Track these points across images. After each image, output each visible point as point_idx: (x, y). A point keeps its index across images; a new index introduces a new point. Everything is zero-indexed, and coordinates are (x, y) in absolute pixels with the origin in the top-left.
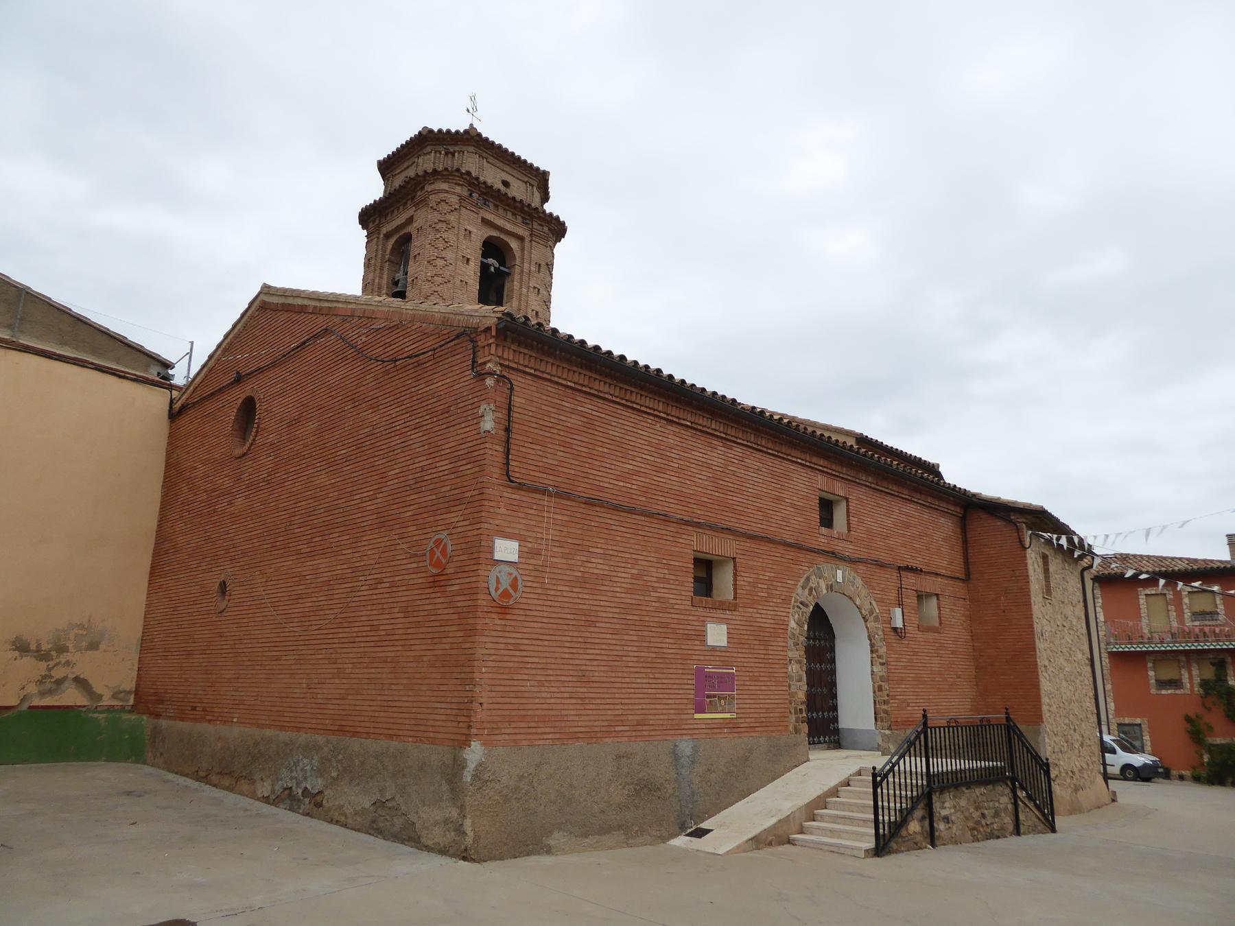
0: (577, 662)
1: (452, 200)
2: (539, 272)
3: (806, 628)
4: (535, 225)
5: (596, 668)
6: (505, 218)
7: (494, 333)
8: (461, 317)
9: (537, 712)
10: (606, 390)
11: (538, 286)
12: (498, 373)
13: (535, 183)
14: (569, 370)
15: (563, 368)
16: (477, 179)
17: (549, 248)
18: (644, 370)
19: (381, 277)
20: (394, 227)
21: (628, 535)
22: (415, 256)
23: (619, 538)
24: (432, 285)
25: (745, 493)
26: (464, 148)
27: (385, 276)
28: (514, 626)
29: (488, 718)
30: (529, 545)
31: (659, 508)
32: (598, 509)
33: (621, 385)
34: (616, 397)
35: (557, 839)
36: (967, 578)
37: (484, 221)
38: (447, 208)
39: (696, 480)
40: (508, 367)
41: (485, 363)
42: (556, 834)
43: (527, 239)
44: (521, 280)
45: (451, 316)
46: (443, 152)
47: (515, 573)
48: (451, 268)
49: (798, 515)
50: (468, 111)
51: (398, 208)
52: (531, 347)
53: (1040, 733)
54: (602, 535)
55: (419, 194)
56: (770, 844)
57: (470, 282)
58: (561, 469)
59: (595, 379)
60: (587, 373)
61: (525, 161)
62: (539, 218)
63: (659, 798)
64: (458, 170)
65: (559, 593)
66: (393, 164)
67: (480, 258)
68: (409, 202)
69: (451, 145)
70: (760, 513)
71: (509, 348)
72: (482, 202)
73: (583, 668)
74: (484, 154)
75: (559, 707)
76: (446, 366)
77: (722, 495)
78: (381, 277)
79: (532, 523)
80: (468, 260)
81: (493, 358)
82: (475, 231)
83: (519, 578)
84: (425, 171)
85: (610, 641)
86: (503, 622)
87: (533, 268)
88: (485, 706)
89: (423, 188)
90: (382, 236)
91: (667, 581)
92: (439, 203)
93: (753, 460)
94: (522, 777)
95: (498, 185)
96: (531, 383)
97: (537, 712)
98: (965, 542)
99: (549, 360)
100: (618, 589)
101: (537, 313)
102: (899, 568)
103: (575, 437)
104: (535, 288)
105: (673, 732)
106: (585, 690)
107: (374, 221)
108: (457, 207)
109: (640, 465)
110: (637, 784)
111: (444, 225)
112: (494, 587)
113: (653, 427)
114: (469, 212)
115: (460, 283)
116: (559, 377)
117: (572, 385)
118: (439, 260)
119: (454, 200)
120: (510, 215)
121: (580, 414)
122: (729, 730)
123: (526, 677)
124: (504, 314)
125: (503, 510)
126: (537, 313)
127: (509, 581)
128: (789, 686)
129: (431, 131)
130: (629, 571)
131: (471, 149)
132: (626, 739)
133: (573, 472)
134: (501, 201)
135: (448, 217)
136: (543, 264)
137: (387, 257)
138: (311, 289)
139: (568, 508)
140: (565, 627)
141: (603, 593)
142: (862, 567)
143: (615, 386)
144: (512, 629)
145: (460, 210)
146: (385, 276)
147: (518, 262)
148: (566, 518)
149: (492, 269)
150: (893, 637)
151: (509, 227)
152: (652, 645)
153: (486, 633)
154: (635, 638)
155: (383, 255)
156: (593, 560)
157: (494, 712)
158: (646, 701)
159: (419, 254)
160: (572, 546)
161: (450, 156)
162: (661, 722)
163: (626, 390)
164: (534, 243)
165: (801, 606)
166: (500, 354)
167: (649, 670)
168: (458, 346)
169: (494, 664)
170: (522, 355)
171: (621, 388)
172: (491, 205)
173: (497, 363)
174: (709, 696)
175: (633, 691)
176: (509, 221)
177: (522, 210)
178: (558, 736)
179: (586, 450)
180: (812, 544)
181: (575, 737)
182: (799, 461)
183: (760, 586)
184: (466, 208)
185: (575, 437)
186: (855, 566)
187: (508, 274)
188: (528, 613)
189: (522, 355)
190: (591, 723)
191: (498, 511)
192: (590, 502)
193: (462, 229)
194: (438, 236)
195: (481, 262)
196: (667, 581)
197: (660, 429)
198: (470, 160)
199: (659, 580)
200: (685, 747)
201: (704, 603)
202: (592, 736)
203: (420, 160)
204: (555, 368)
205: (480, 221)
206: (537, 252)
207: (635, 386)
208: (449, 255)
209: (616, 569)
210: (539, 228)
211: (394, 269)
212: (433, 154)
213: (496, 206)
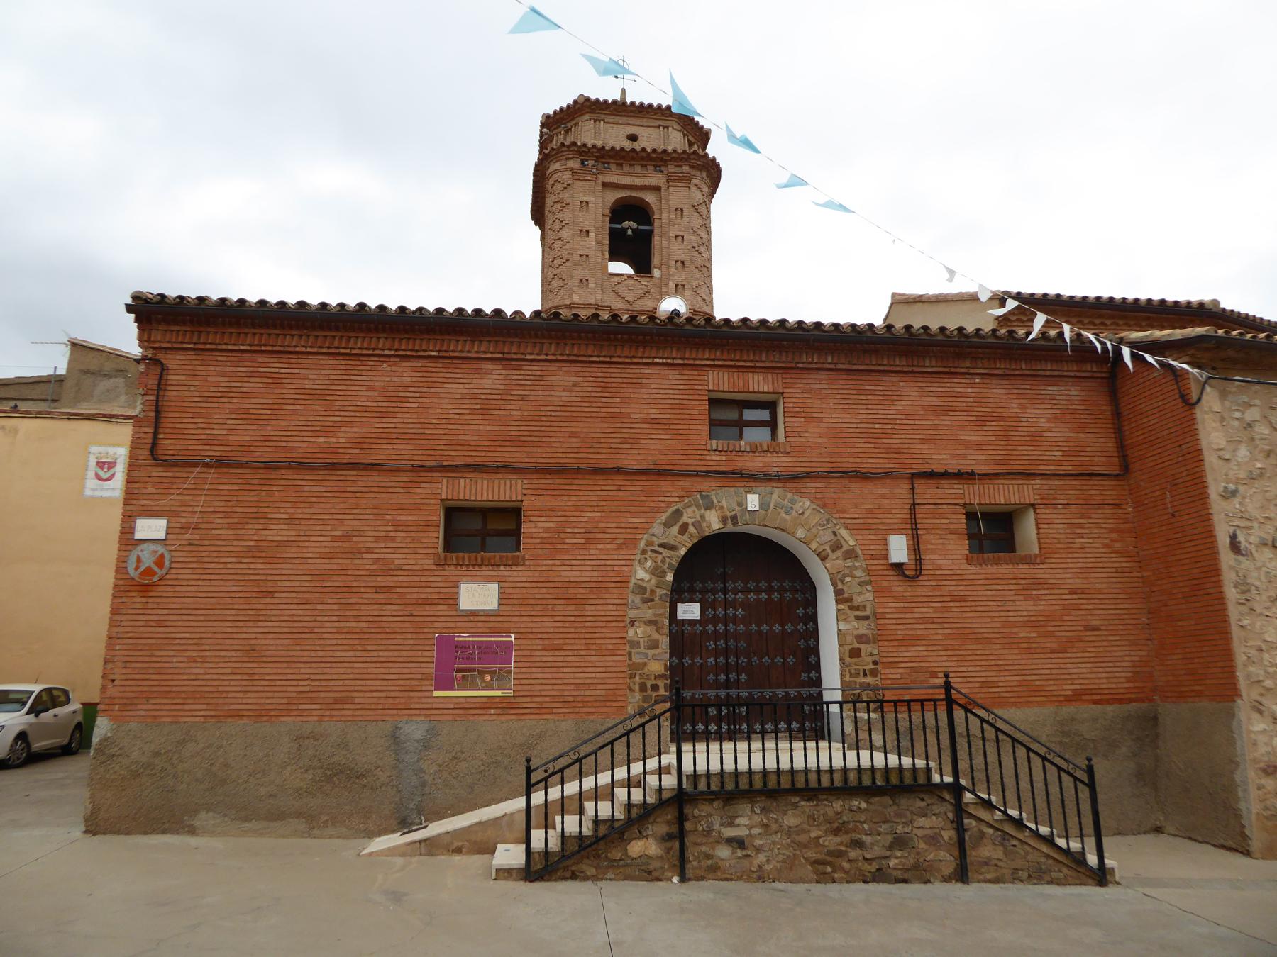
0: (244, 636)
3: (670, 577)
5: (272, 642)
6: (630, 174)
9: (184, 689)
12: (150, 356)
21: (329, 495)
23: (314, 499)
25: (544, 419)
28: (158, 603)
29: (120, 695)
30: (183, 520)
31: (381, 458)
32: (283, 472)
35: (203, 819)
36: (1124, 470)
37: (604, 185)
39: (451, 416)
42: (203, 815)
47: (161, 549)
48: (568, 246)
49: (660, 431)
52: (184, 323)
53: (1234, 715)
54: (288, 499)
56: (458, 851)
57: (591, 253)
58: (231, 437)
61: (650, 106)
62: (673, 159)
63: (365, 786)
65: (221, 566)
70: (574, 440)
73: (253, 642)
75: (216, 683)
77: (502, 428)
79: (187, 498)
80: (588, 232)
83: (167, 555)
85: (294, 612)
86: (144, 600)
87: (672, 216)
88: (116, 683)
91: (393, 539)
93: (560, 377)
94: (157, 754)
95: (628, 145)
96: (194, 357)
97: (184, 689)
98: (1117, 414)
99: (209, 329)
100: (310, 555)
101: (683, 262)
102: (914, 476)
103: (253, 401)
104: (677, 237)
105: (395, 712)
106: (255, 665)
109: (353, 414)
110: (327, 769)
112: (134, 566)
113: (380, 368)
114: (584, 183)
117: (248, 348)
119: (566, 176)
121: (262, 375)
122: (499, 711)
123: (171, 653)
125: (151, 490)
127: (153, 559)
128: (630, 655)
130: (328, 533)
131: (587, 117)
132: (316, 719)
133: (248, 438)
134: (623, 158)
136: (686, 208)
138: (937, 292)
139: (241, 476)
140: (229, 600)
141: (288, 561)
142: (812, 486)
144: (155, 606)
148: (236, 487)
149: (630, 232)
150: (895, 578)
151: (638, 181)
152: (363, 613)
153: (124, 611)
154: (335, 607)
156: (273, 527)
157: (127, 689)
158: (351, 676)
160: (243, 515)
162: (375, 700)
165: (661, 550)
167: (356, 642)
169: (131, 641)
172: (613, 167)
174: (459, 671)
175: (329, 665)
176: (637, 175)
177: (651, 159)
178: (212, 713)
179: (269, 412)
180: (694, 464)
181: (237, 714)
182: (657, 360)
183: (569, 530)
185: (253, 401)
186: (795, 485)
188: (178, 588)
190: (263, 701)
191: (145, 491)
192: (272, 466)
196: (393, 539)
197: (389, 369)
199: (377, 539)
200: (415, 730)
201: (479, 559)
202: (261, 714)
205: (600, 187)
206: (677, 197)
208: (565, 233)
209: (307, 533)
210: (678, 170)
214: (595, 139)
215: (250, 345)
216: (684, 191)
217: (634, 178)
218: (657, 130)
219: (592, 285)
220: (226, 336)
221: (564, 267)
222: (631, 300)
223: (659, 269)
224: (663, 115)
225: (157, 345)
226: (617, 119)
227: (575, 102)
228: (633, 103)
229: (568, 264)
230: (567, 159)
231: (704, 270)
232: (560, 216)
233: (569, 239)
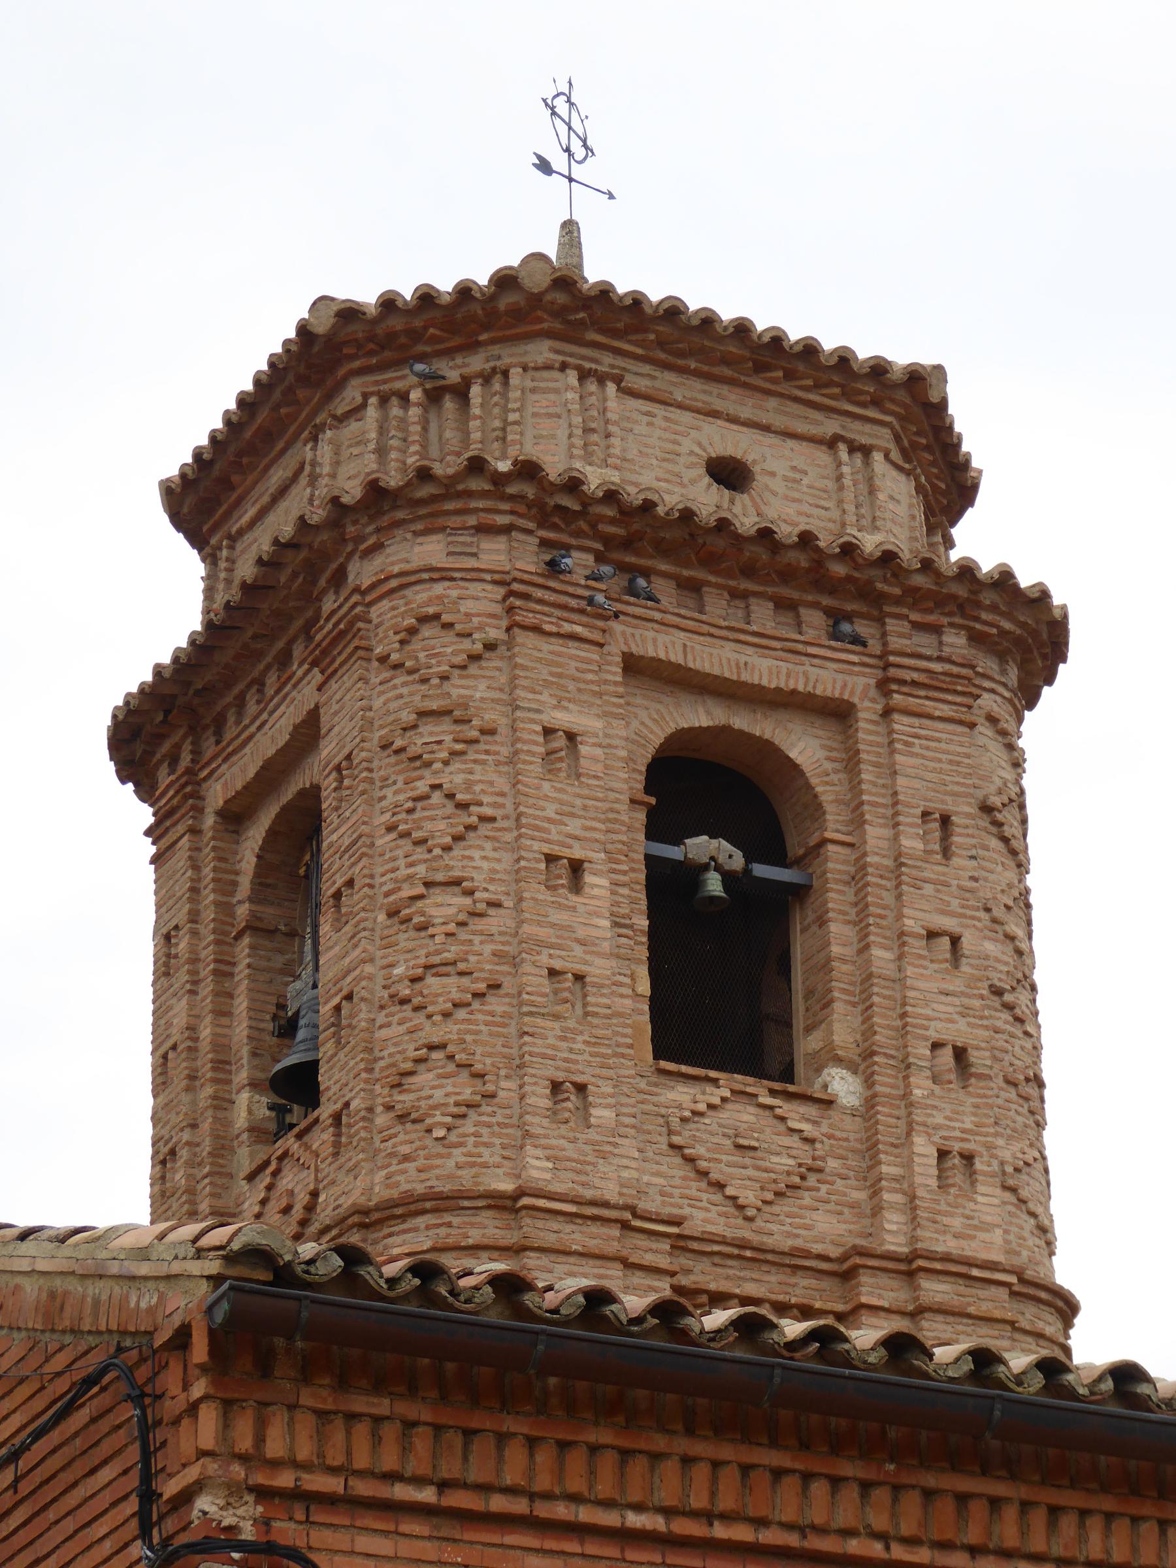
1: (467, 606)
2: (946, 852)
4: (900, 635)
6: (736, 635)
7: (200, 1351)
8: (94, 1289)
10: (844, 1516)
11: (948, 923)
12: (248, 1533)
13: (882, 437)
14: (625, 1454)
15: (594, 1449)
16: (573, 485)
17: (984, 729)
18: (1037, 1381)
19: (222, 1013)
20: (251, 773)
22: (337, 895)
24: (419, 1018)
26: (508, 355)
27: (241, 1004)
33: (930, 1480)
34: (911, 1542)
38: (451, 648)
40: (298, 1495)
41: (186, 1497)
43: (867, 711)
44: (861, 904)
45: (73, 1285)
46: (415, 395)
48: (496, 922)
50: (544, 166)
51: (260, 683)
55: (328, 605)
57: (599, 968)
59: (778, 1474)
60: (726, 1452)
61: (810, 349)
62: (914, 598)
64: (477, 465)
66: (226, 484)
67: (640, 845)
68: (298, 651)
69: (449, 353)
71: (292, 1407)
72: (618, 583)
74: (606, 363)
76: (69, 1525)
78: (222, 1013)
80: (577, 868)
81: (212, 1467)
82: (597, 724)
84: (335, 501)
87: (911, 843)
89: (339, 577)
90: (209, 820)
92: (412, 631)
99: (510, 1424)
101: (960, 1054)
104: (932, 935)
107: (173, 759)
108: (494, 634)
111: (443, 731)
114: (556, 645)
115: (546, 986)
116: (575, 1498)
117: (658, 1523)
118: (438, 896)
120: (763, 616)
124: (231, 1259)
126: (960, 1054)
129: (349, 313)
131: (541, 351)
134: (710, 560)
135: (457, 689)
136: (963, 811)
137: (243, 911)
143: (897, 1489)
145: (510, 645)
146: (241, 1004)
147: (834, 823)
149: (714, 885)
155: (225, 908)
159: (350, 883)
161: (449, 404)
163: (962, 1499)
164: (902, 723)
166: (245, 1444)
168: (104, 1425)
170: (362, 1430)
171: (929, 1494)
172: (664, 589)
173: (234, 1491)
176: (762, 642)
184: (536, 629)
187: (800, 892)
189: (362, 1430)
193: (531, 732)
194: (422, 787)
195: (649, 858)
198: (540, 403)
203: (325, 451)
204: (544, 1457)
205: (615, 673)
207: (1012, 1470)
210: (924, 643)
211: (279, 961)
212: (372, 412)
213: (691, 587)
214: (588, 458)
215: (668, 1512)
216: (951, 739)
217: (750, 656)
218: (822, 456)
219: (602, 1114)
220: (576, 1461)
221: (479, 1012)
222: (749, 1196)
223: (853, 1068)
224: (848, 394)
225: (285, 1480)
226: (665, 381)
227: (505, 280)
228: (605, 291)
229: (496, 1004)
230: (483, 529)
231: (1031, 1090)
232: (454, 777)
233: (496, 891)
